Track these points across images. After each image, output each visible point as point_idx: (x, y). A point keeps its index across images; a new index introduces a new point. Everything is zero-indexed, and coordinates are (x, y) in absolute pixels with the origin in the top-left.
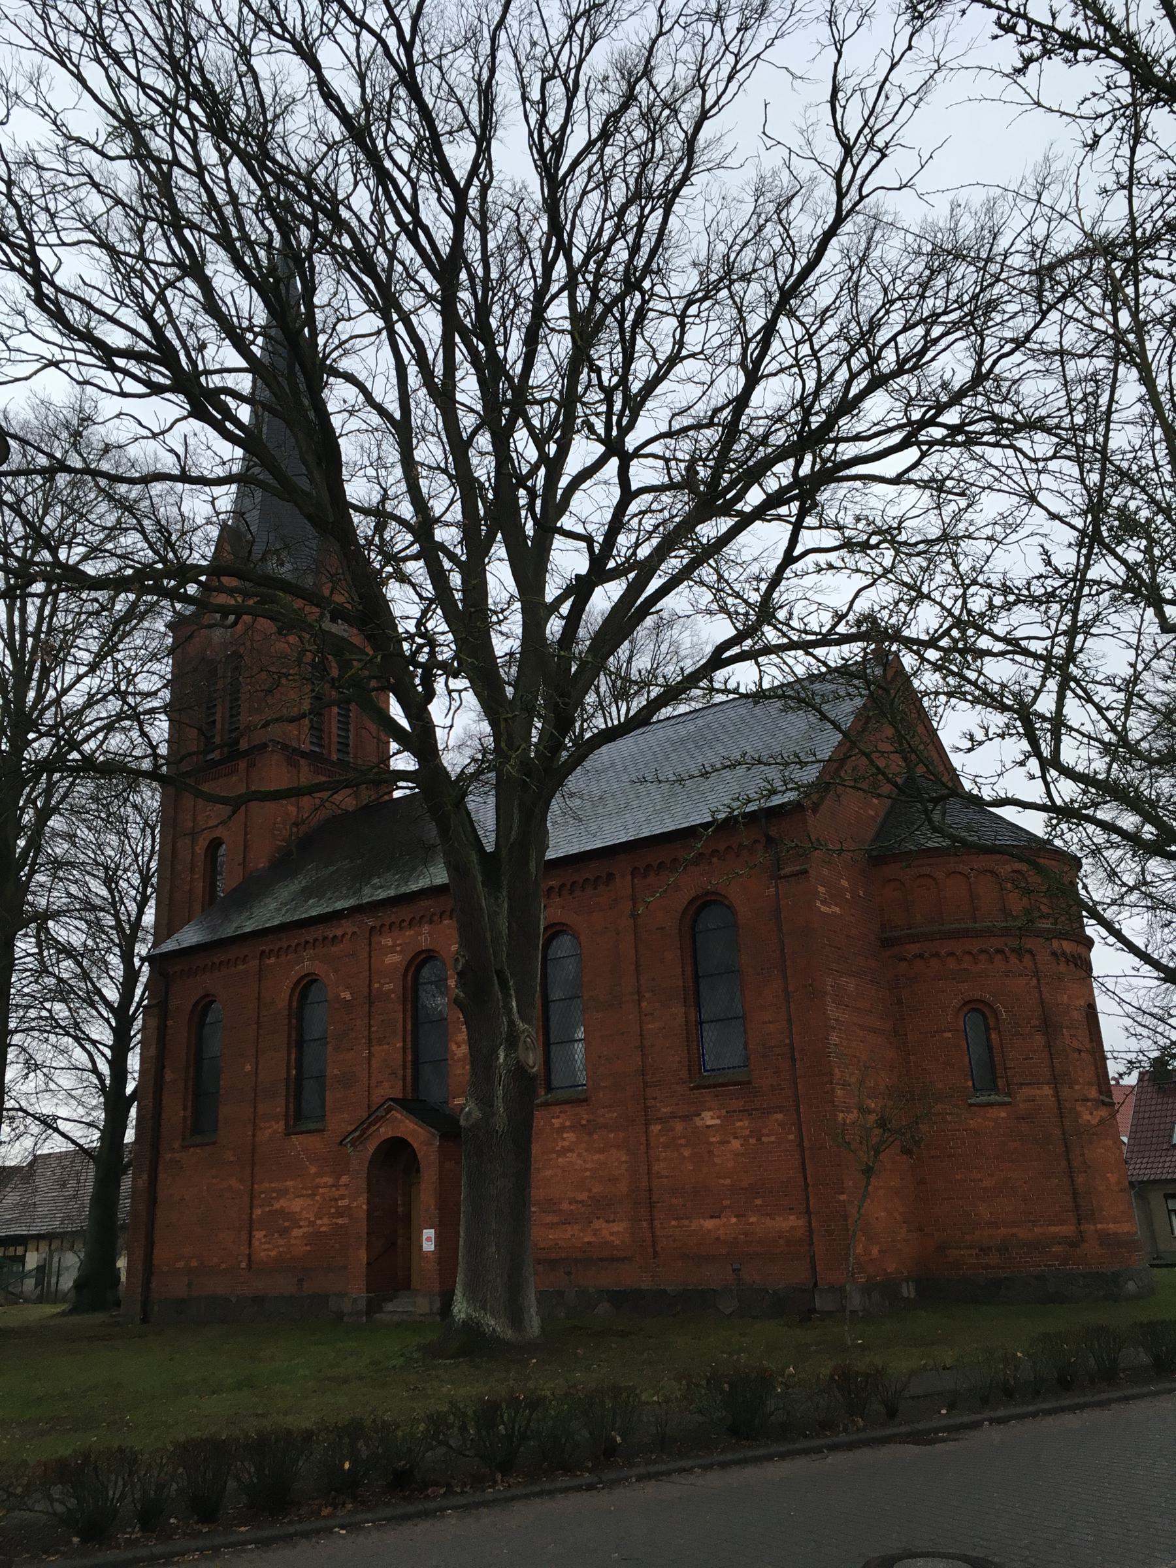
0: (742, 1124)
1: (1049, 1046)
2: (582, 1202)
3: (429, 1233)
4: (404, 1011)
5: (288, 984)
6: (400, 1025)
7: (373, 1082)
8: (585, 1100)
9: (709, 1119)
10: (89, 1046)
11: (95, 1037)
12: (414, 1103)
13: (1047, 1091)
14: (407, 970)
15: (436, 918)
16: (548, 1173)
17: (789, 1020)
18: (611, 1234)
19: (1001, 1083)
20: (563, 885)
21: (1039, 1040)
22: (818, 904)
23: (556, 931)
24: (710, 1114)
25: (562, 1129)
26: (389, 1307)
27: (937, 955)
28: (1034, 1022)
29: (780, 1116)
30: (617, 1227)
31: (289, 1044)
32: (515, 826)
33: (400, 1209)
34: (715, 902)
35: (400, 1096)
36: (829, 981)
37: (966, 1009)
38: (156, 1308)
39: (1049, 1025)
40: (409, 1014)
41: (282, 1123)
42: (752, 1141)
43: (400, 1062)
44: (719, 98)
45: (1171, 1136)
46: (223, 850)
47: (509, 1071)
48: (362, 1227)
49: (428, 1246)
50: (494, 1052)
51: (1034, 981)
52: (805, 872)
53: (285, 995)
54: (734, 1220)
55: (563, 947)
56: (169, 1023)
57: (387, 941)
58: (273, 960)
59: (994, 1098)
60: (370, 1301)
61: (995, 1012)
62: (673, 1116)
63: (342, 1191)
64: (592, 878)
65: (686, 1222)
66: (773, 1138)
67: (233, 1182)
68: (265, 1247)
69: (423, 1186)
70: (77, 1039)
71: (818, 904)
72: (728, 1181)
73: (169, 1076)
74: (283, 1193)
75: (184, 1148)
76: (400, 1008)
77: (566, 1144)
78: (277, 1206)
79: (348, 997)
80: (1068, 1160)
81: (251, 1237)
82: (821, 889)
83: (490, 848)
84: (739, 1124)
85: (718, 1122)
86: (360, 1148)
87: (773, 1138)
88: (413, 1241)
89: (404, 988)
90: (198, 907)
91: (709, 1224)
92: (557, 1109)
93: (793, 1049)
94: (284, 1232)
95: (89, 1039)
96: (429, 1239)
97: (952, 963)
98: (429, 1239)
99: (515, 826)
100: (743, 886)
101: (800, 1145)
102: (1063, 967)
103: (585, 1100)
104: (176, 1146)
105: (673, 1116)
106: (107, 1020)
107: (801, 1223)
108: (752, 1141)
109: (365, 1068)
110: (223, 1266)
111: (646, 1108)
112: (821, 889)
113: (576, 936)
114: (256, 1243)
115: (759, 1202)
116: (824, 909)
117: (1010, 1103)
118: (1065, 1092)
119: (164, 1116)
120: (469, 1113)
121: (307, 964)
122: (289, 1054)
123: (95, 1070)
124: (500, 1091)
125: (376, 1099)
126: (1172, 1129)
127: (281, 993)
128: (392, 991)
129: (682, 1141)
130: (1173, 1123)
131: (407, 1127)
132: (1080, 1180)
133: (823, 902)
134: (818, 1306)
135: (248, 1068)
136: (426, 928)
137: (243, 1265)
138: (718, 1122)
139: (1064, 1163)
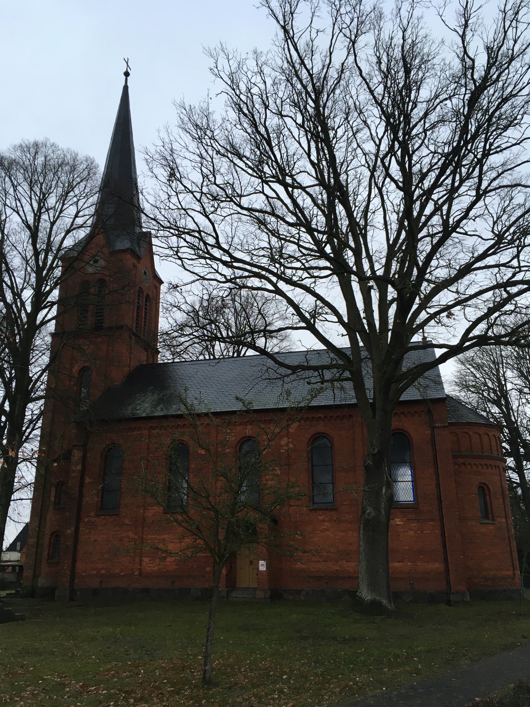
8: (336, 509)
19: (490, 516)
25: (324, 521)
29: (431, 523)
38: (78, 593)
50: (381, 489)
56: (88, 455)
59: (488, 521)
61: (489, 489)
67: (131, 534)
68: (150, 565)
75: (97, 516)
80: (510, 547)
81: (141, 561)
84: (412, 525)
85: (403, 523)
92: (321, 512)
96: (262, 565)
98: (262, 565)
103: (336, 509)
104: (93, 514)
110: (122, 574)
114: (144, 564)
115: (422, 557)
120: (370, 513)
124: (383, 506)
134: (451, 600)
137: (136, 573)
138: (403, 523)
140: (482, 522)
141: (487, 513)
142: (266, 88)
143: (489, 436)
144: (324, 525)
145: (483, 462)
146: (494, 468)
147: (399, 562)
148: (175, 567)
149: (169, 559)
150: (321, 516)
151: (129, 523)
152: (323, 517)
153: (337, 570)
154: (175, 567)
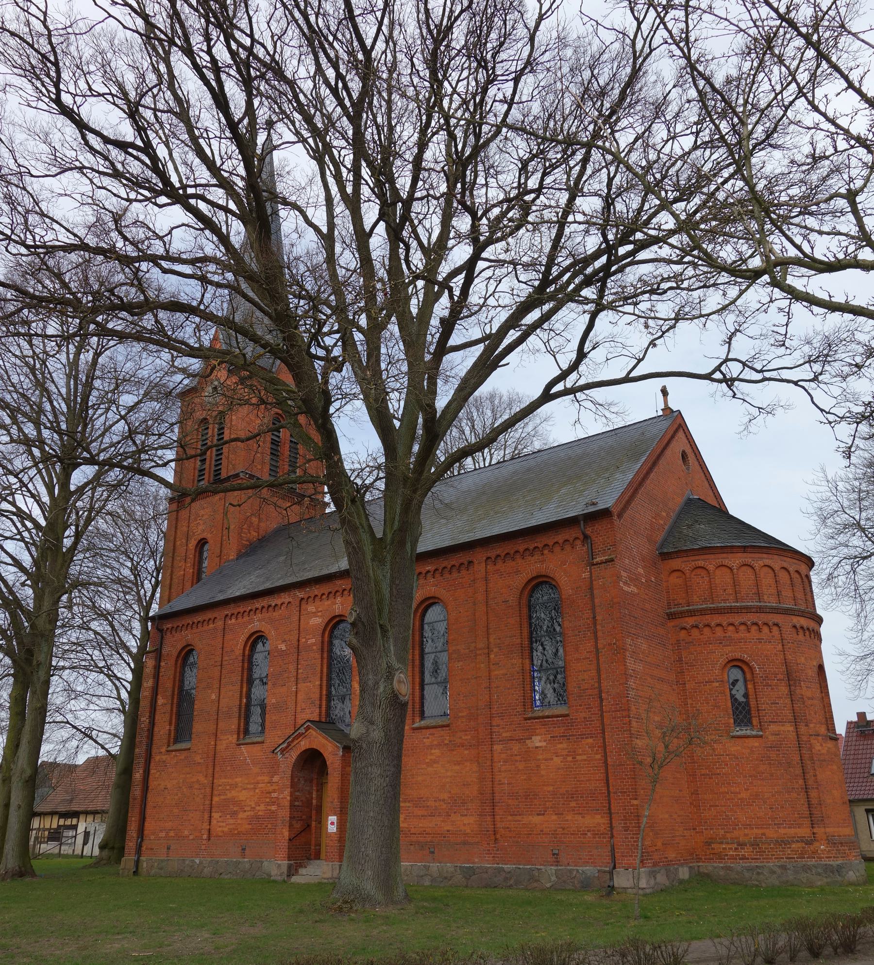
0: (563, 746)
1: (791, 694)
2: (444, 800)
3: (333, 818)
4: (322, 658)
5: (243, 638)
6: (318, 669)
7: (299, 709)
9: (537, 741)
10: (117, 682)
11: (119, 675)
12: (327, 723)
13: (790, 727)
14: (324, 630)
15: (346, 592)
16: (420, 779)
17: (599, 671)
18: (464, 825)
19: (755, 721)
20: (436, 570)
21: (784, 690)
22: (621, 584)
23: (429, 602)
24: (539, 738)
26: (302, 871)
27: (708, 626)
28: (780, 676)
29: (590, 741)
30: (466, 820)
31: (242, 680)
32: (397, 518)
33: (314, 802)
34: (546, 582)
35: (317, 719)
36: (629, 641)
37: (729, 665)
39: (791, 678)
40: (325, 661)
41: (235, 736)
42: (570, 759)
43: (318, 696)
44: (552, 5)
45: (870, 768)
46: (206, 547)
47: (387, 698)
48: (284, 813)
49: (332, 829)
51: (780, 646)
52: (612, 560)
53: (240, 646)
54: (554, 817)
55: (434, 614)
56: (163, 664)
57: (311, 608)
58: (233, 621)
60: (290, 867)
61: (751, 668)
62: (511, 739)
63: (275, 787)
64: (457, 565)
65: (518, 818)
66: (585, 757)
69: (330, 785)
70: (108, 676)
71: (621, 584)
72: (551, 788)
73: (160, 701)
74: (234, 786)
76: (318, 656)
77: (433, 757)
78: (229, 795)
79: (284, 648)
82: (624, 574)
83: (379, 535)
85: (544, 744)
86: (287, 755)
87: (585, 757)
88: (321, 822)
89: (323, 642)
90: (188, 584)
91: (536, 819)
93: (600, 692)
94: (234, 814)
95: (115, 676)
97: (719, 632)
98: (332, 823)
99: (397, 518)
100: (565, 567)
101: (606, 762)
102: (801, 637)
104: (163, 750)
105: (511, 739)
106: (128, 664)
107: (602, 821)
108: (570, 759)
109: (292, 697)
111: (491, 733)
112: (624, 574)
113: (445, 606)
114: (214, 822)
115: (573, 804)
116: (626, 588)
117: (761, 736)
118: (803, 729)
119: (156, 729)
121: (257, 623)
122: (242, 687)
123: (119, 698)
125: (300, 722)
126: (871, 763)
127: (238, 642)
128: (314, 644)
129: (518, 758)
130: (871, 759)
131: (318, 740)
132: (813, 794)
133: (625, 583)
135: (213, 697)
136: (339, 599)
137: (205, 837)
138: (544, 744)
139: (801, 782)
140: (736, 733)
141: (743, 713)
142: (21, 38)
143: (788, 572)
144: (432, 754)
145: (737, 619)
146: (766, 630)
147: (538, 815)
148: (247, 826)
149: (241, 815)
150: (428, 738)
151: (200, 761)
152: (430, 740)
153: (448, 831)
154: (247, 826)
